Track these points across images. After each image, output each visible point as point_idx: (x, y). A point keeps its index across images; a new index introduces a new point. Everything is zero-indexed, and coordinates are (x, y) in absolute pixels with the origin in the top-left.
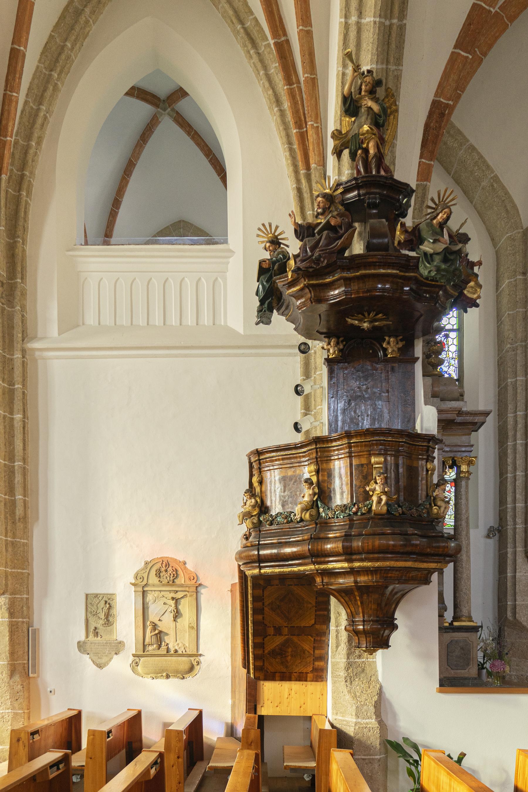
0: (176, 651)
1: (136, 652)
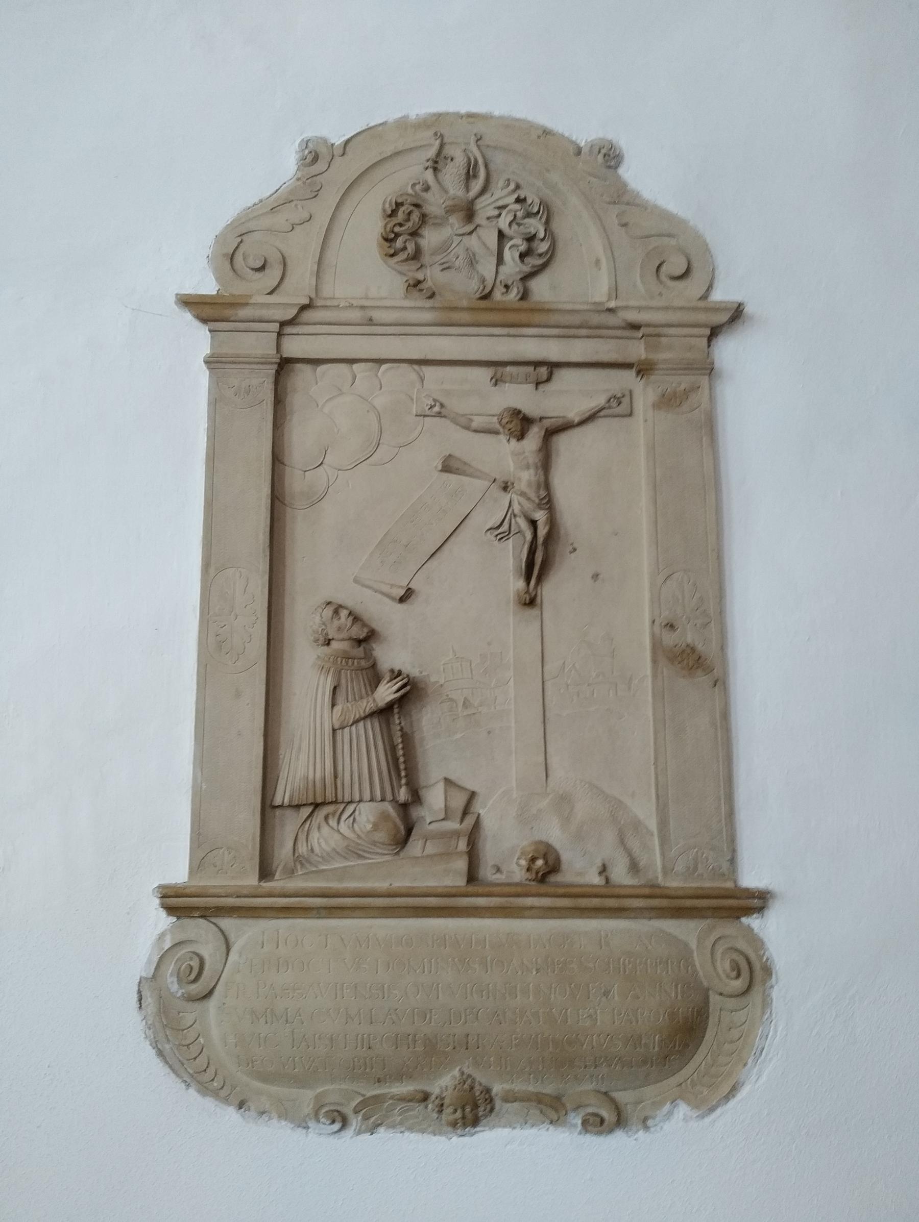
0: (546, 867)
1: (197, 866)
